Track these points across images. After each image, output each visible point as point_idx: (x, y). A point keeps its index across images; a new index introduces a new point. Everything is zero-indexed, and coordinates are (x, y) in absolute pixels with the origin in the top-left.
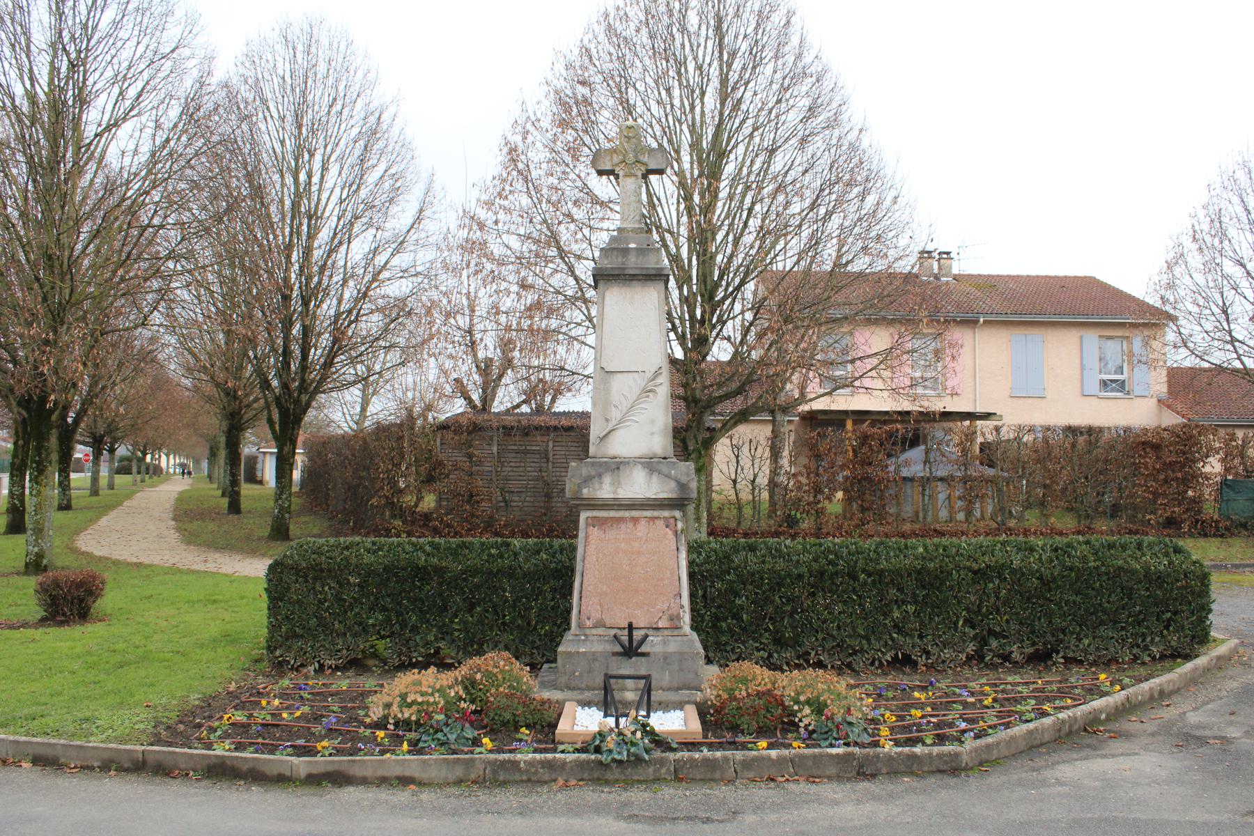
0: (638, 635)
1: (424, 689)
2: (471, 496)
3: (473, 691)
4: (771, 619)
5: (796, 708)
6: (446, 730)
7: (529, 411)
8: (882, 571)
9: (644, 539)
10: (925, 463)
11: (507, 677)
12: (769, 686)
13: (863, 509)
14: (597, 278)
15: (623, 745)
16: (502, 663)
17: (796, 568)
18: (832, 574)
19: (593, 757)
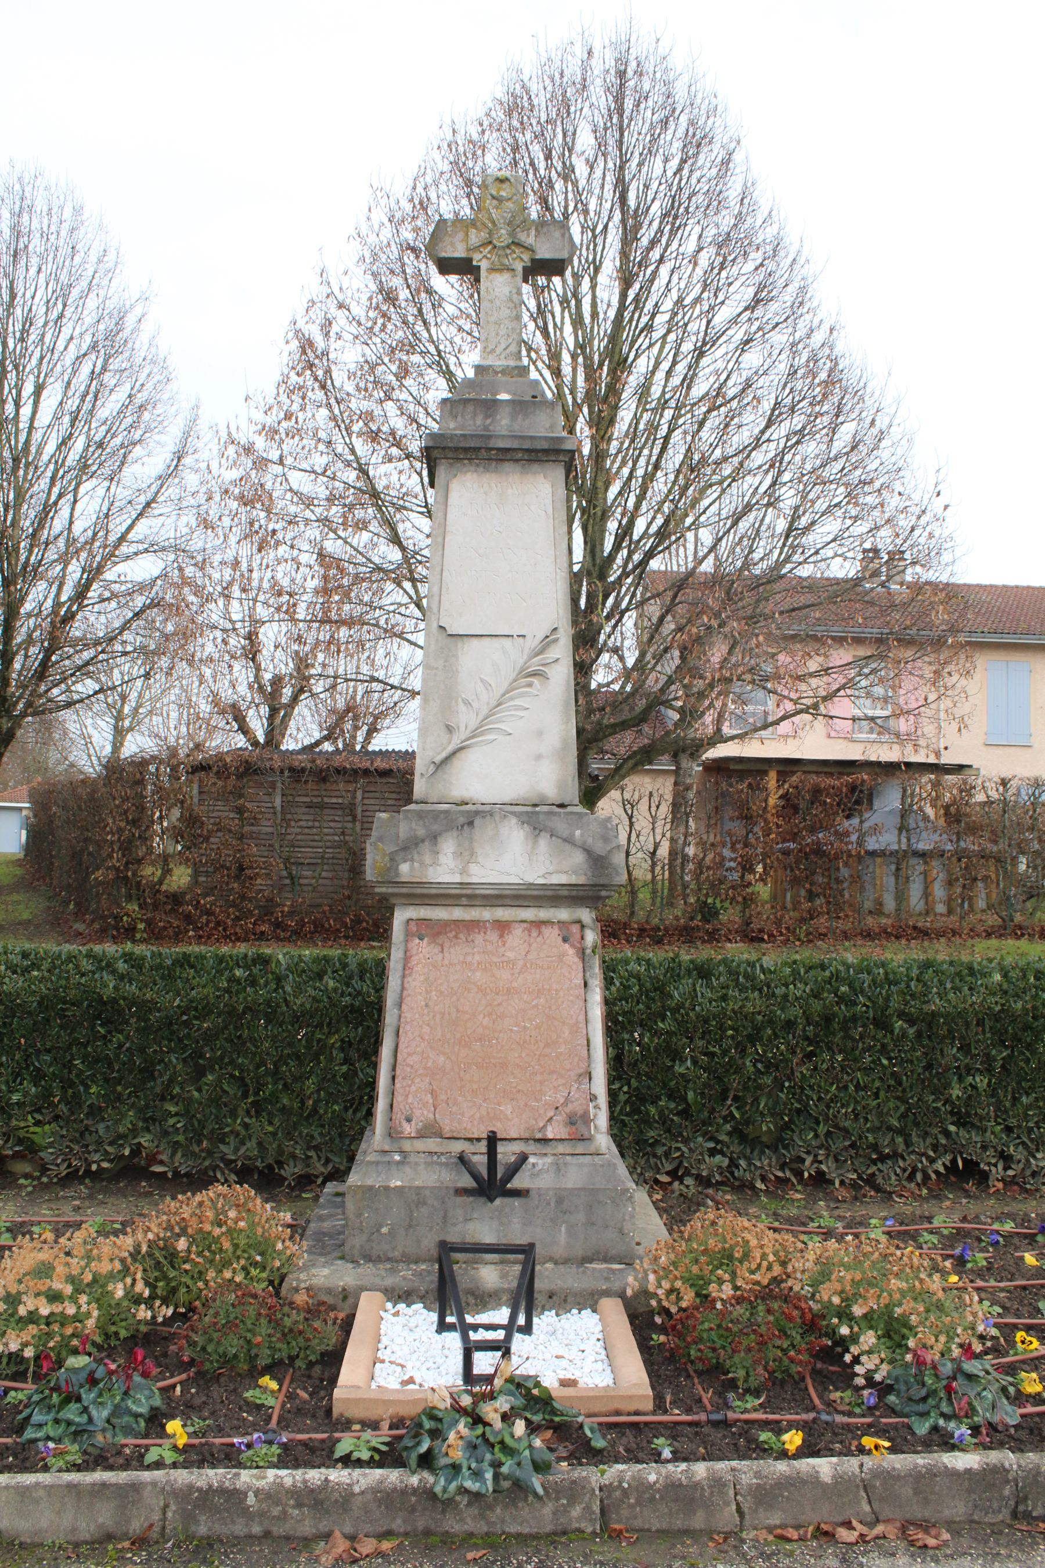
0: (506, 1153)
1: (57, 1285)
2: (241, 869)
3: (172, 1274)
4: (736, 1098)
5: (844, 1330)
6: (88, 1396)
7: (331, 749)
8: (934, 1015)
9: (521, 963)
10: (900, 830)
11: (242, 1242)
12: (777, 1270)
13: (811, 896)
14: (435, 454)
15: (483, 1448)
16: (232, 1214)
17: (782, 1009)
18: (845, 1021)
19: (414, 1480)
